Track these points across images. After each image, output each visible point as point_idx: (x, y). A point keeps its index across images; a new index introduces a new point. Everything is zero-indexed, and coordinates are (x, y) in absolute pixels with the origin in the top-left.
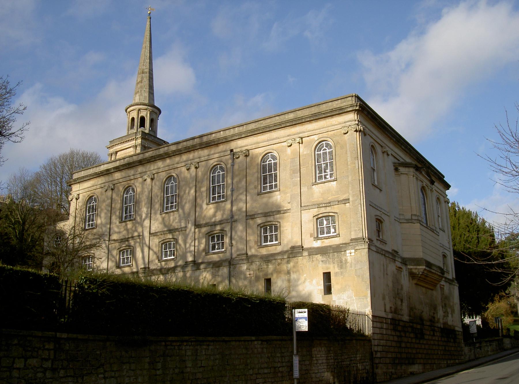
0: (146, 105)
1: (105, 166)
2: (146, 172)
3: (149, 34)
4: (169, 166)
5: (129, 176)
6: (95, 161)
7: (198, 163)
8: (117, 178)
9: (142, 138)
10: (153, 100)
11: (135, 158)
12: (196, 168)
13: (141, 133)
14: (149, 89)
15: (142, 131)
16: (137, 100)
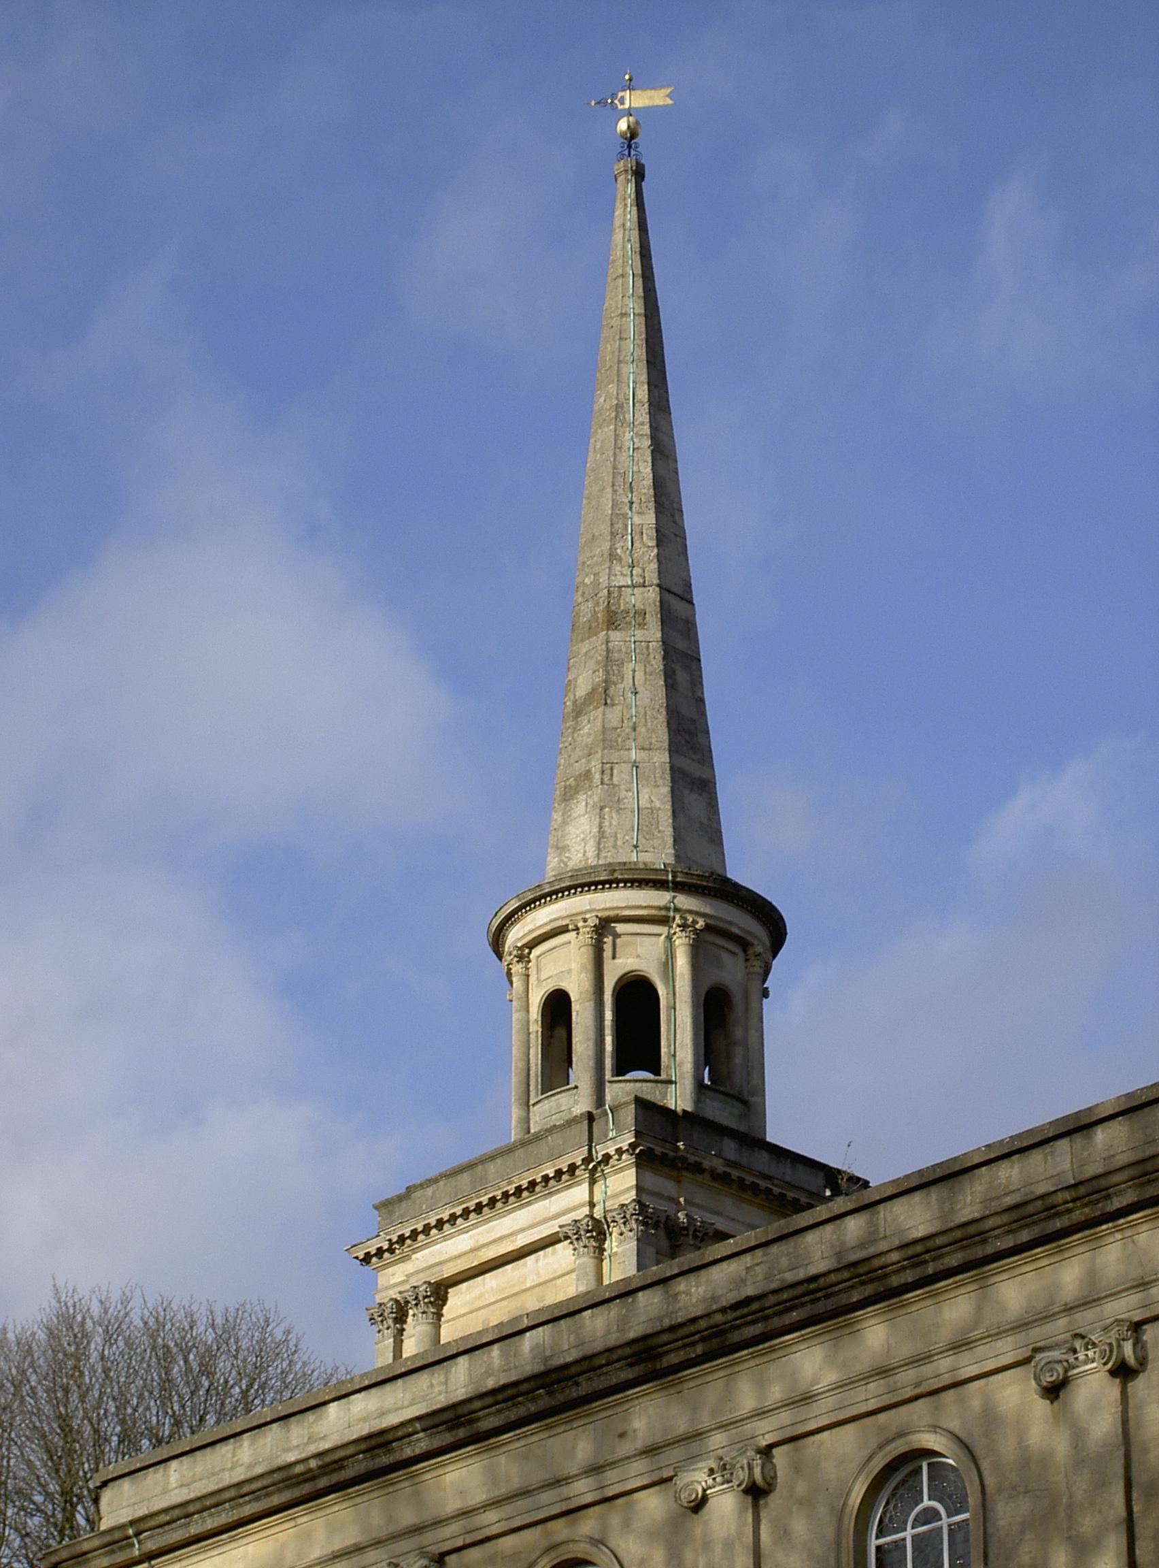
0: (660, 885)
1: (361, 1405)
2: (696, 1436)
3: (635, 306)
4: (883, 1372)
5: (559, 1482)
6: (254, 1380)
7: (1137, 1327)
8: (453, 1505)
9: (646, 1160)
10: (715, 837)
11: (599, 1328)
12: (1123, 1372)
13: (629, 1115)
14: (673, 749)
15: (640, 1103)
16: (579, 840)
